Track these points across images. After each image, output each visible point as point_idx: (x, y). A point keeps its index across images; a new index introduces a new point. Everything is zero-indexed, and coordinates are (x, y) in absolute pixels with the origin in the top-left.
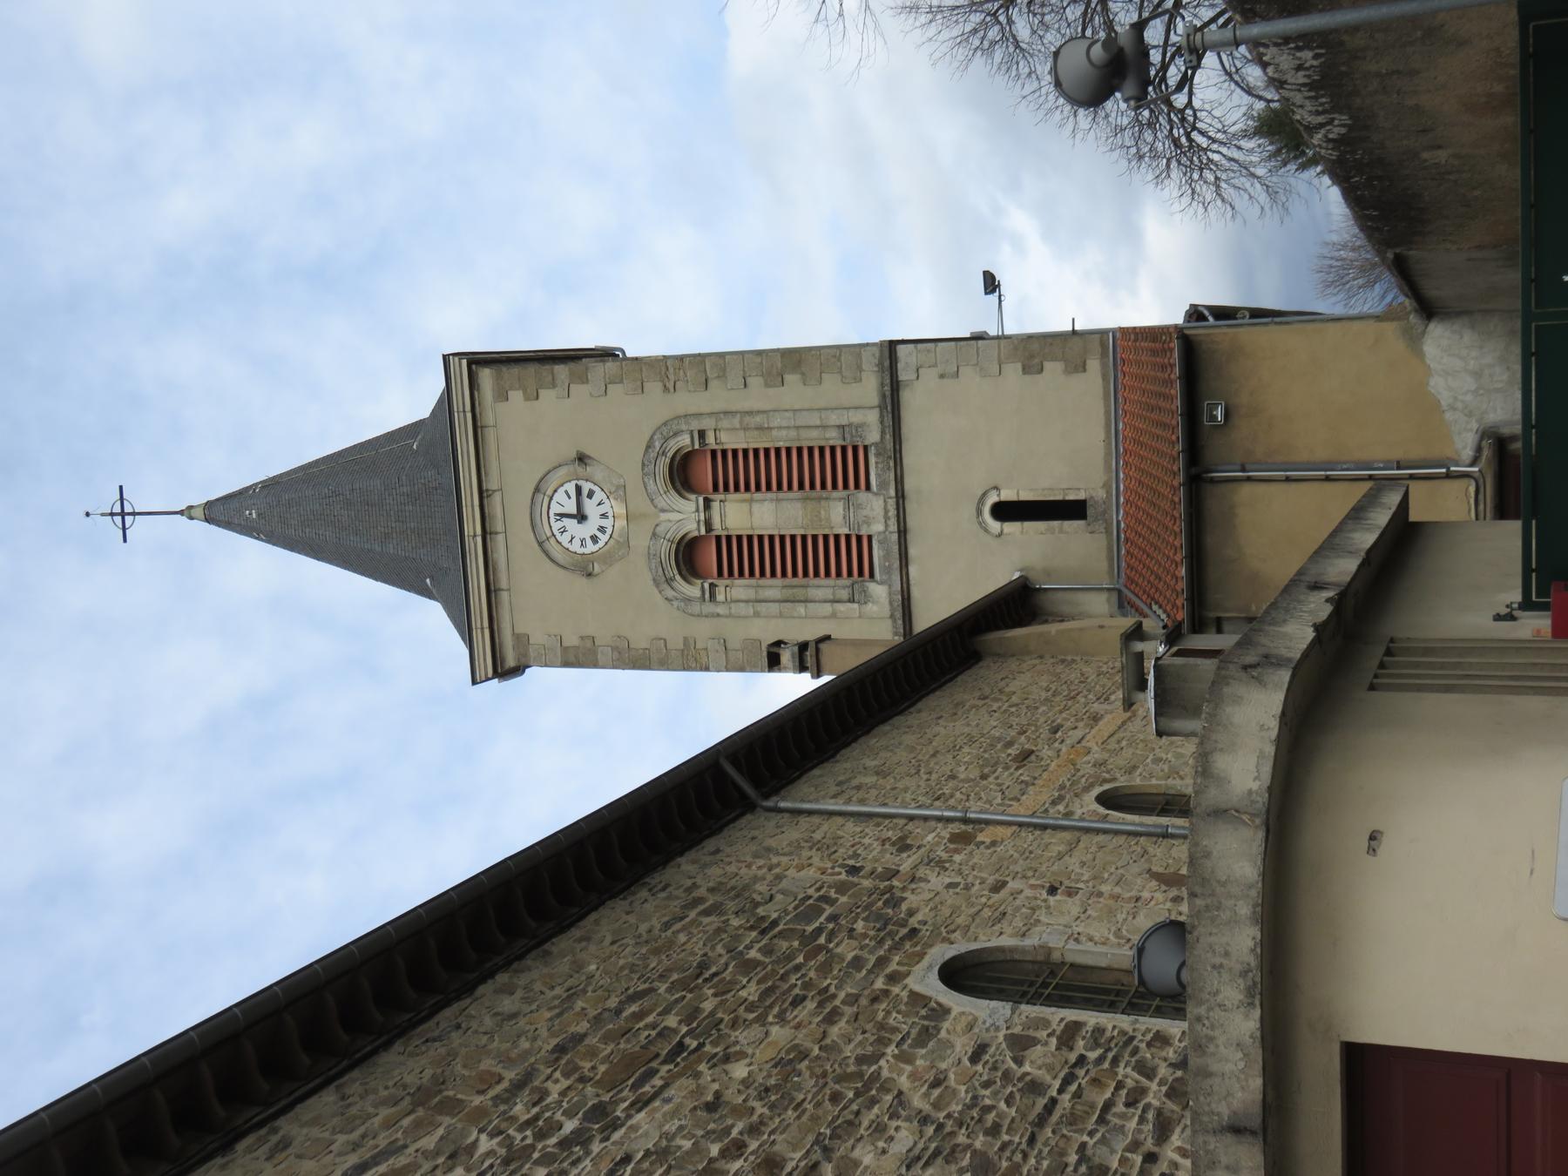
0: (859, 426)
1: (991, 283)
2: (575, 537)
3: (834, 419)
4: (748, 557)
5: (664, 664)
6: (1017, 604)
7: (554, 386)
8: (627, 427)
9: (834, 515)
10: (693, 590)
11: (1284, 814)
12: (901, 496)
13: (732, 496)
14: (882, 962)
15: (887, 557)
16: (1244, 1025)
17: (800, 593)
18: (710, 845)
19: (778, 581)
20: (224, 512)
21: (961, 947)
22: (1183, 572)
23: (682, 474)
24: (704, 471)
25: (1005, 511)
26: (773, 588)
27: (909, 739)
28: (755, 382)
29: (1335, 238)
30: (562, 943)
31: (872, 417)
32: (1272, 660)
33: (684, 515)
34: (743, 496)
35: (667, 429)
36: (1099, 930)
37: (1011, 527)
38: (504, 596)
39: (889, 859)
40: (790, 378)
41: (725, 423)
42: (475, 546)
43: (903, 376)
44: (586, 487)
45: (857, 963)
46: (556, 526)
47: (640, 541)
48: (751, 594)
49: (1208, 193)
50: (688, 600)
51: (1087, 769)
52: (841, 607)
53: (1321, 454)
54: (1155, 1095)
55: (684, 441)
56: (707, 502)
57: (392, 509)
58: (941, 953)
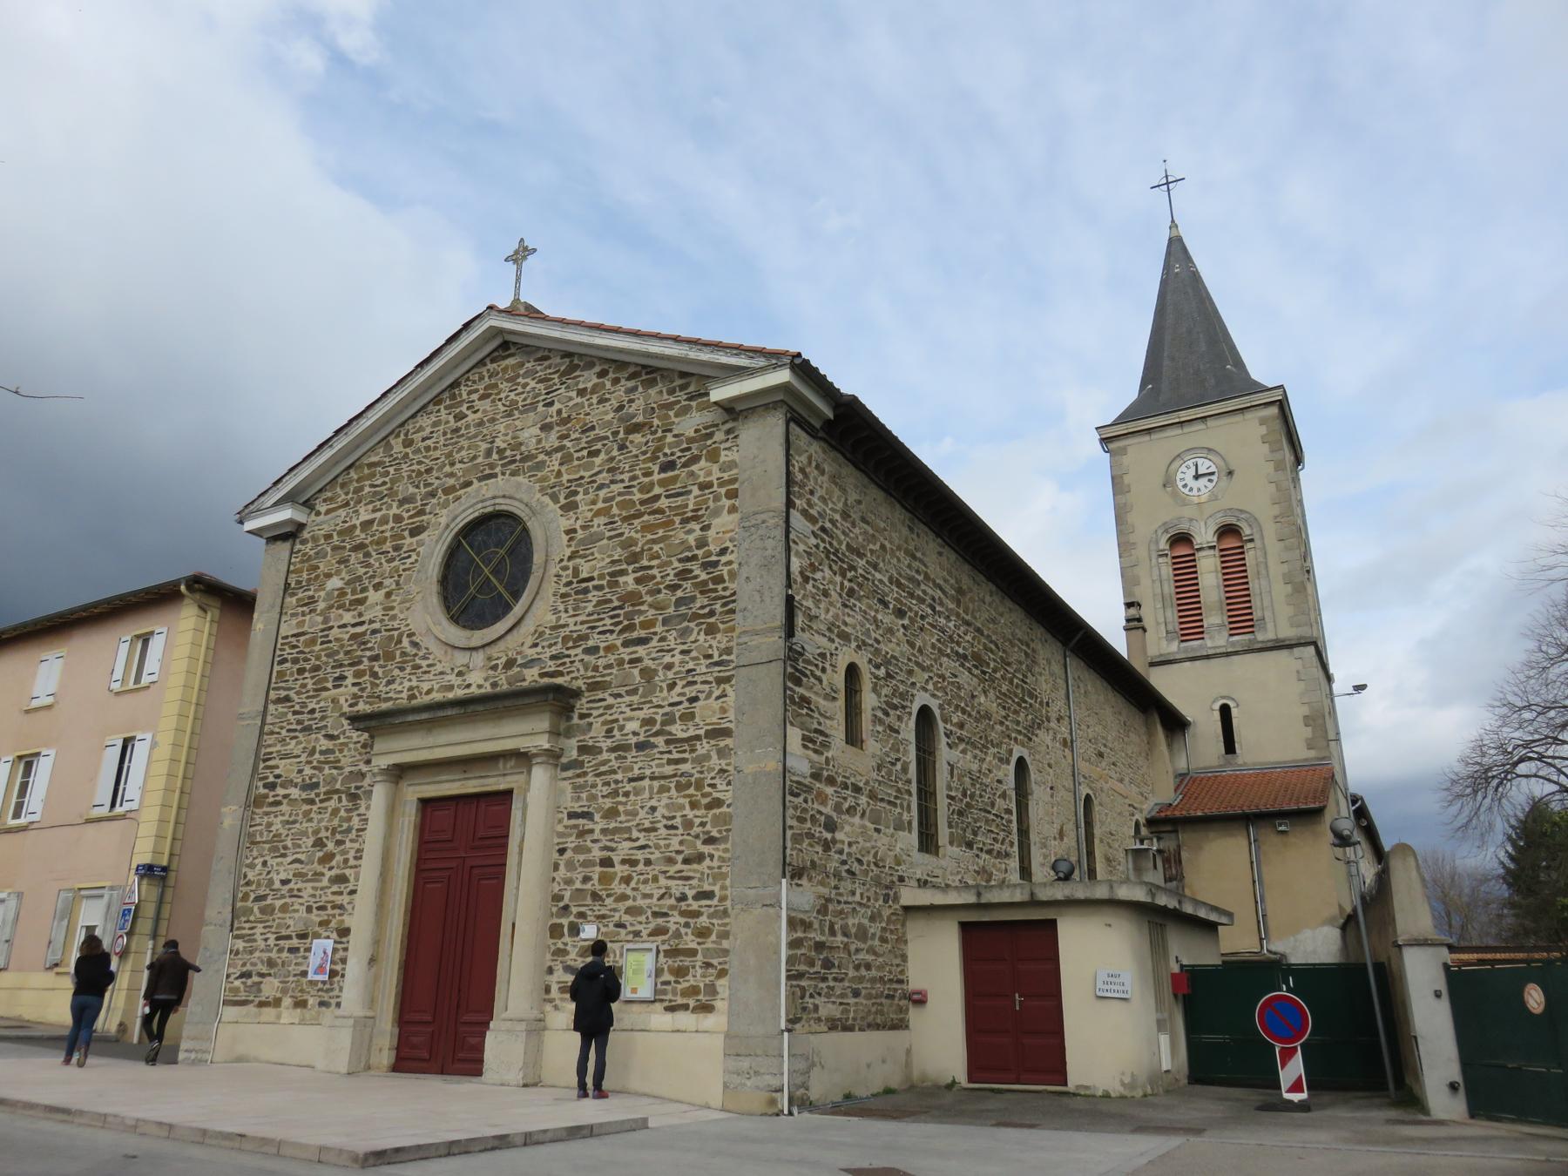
0: (1265, 629)
1: (1360, 688)
2: (1185, 475)
3: (1268, 615)
4: (1185, 572)
5: (1120, 533)
6: (1175, 723)
7: (1272, 451)
8: (1253, 499)
9: (1214, 619)
10: (1163, 544)
11: (1113, 903)
12: (1228, 654)
13: (1218, 560)
14: (1020, 732)
15: (1193, 649)
16: (1059, 896)
17: (1168, 603)
18: (1049, 636)
19: (1173, 590)
20: (1177, 250)
21: (1028, 760)
22: (1199, 813)
23: (1228, 531)
24: (1230, 543)
25: (1225, 711)
26: (1169, 588)
27: (1102, 698)
28: (1285, 567)
29: (1458, 862)
30: (1009, 603)
31: (1270, 635)
32: (1153, 896)
33: (1204, 535)
34: (1219, 566)
35: (1254, 521)
36: (1041, 812)
37: (1217, 715)
38: (1147, 438)
39: (1053, 716)
40: (1289, 587)
41: (1259, 553)
42: (1173, 418)
43: (1296, 650)
44: (1214, 478)
45: (1018, 723)
46: (1190, 463)
47: (1188, 512)
48: (1164, 576)
49: (1457, 789)
50: (1157, 543)
51: (1098, 785)
52: (1163, 627)
53: (1265, 877)
54: (997, 846)
55: (1246, 531)
56: (1213, 547)
57: (1192, 363)
58: (1026, 754)
